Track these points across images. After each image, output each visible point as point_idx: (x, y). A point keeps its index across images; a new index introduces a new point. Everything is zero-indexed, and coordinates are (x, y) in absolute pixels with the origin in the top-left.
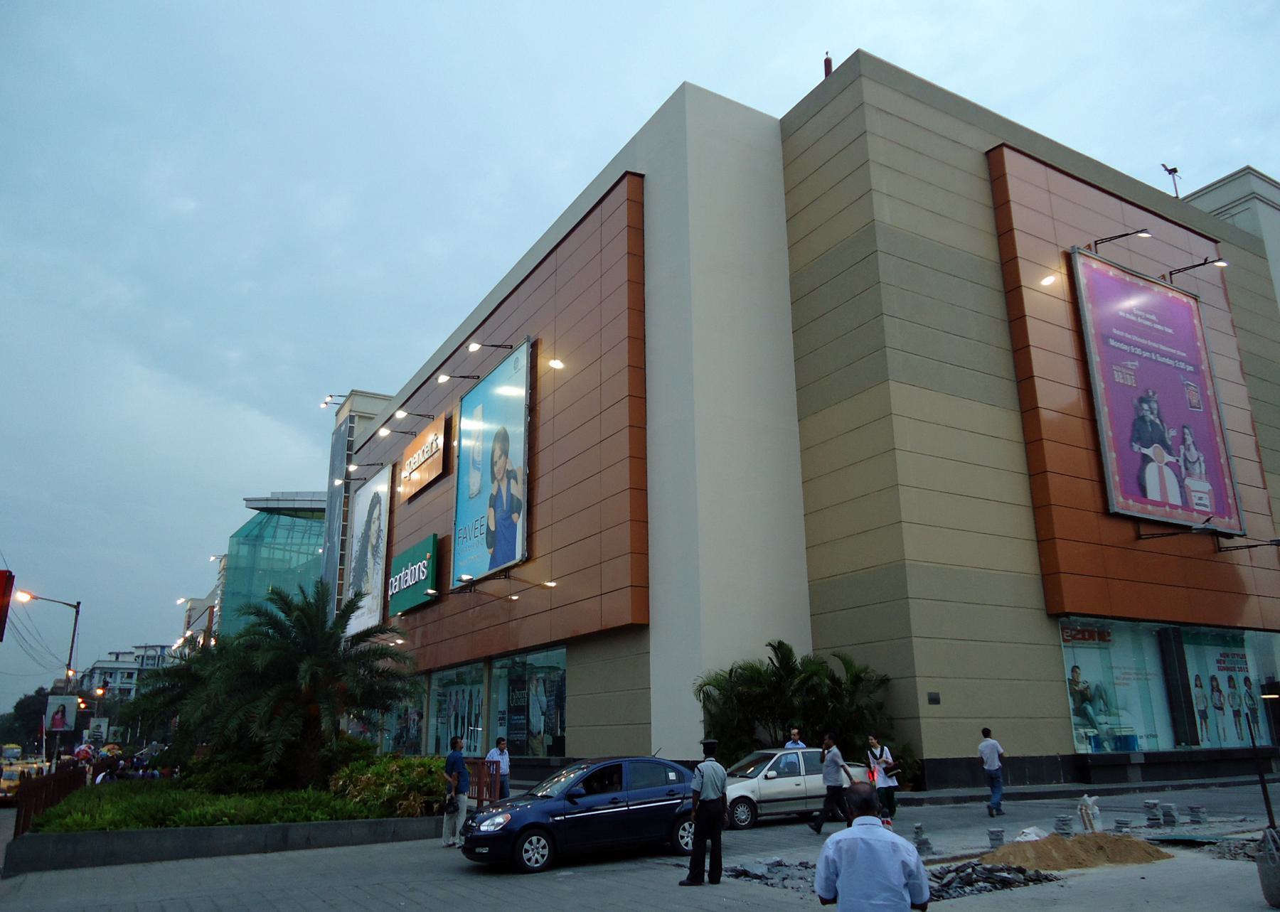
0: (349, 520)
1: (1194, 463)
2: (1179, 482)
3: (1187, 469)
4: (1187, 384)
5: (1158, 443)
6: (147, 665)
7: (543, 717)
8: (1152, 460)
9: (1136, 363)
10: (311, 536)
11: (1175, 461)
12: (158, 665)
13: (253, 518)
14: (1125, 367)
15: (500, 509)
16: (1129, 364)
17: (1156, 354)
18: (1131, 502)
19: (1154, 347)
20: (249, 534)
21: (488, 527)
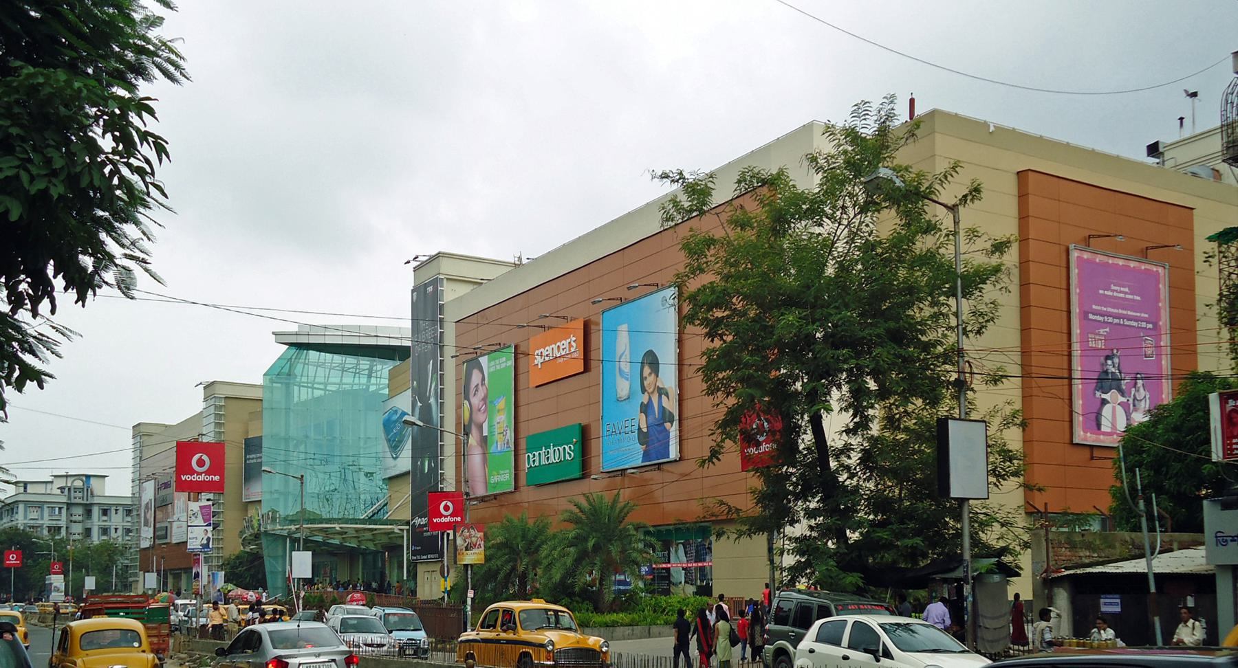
0: (445, 384)
1: (1141, 400)
2: (1127, 416)
3: (1134, 405)
4: (1146, 339)
5: (1116, 389)
6: (75, 498)
7: (684, 571)
8: (1108, 402)
9: (1108, 330)
10: (361, 376)
11: (1126, 401)
12: (87, 500)
13: (282, 355)
14: (1099, 334)
15: (651, 416)
16: (1102, 331)
17: (1124, 319)
18: (1089, 434)
19: (1124, 314)
20: (280, 372)
21: (639, 429)
